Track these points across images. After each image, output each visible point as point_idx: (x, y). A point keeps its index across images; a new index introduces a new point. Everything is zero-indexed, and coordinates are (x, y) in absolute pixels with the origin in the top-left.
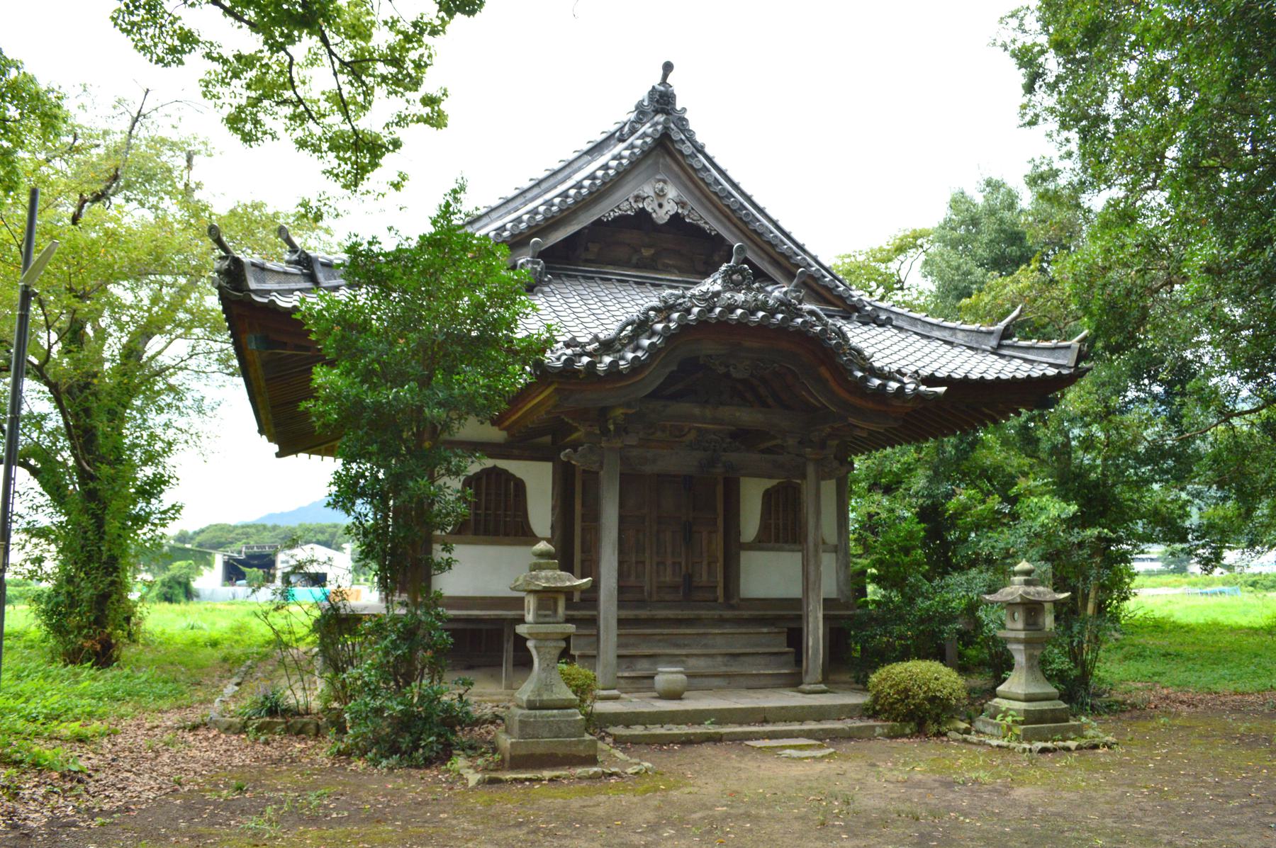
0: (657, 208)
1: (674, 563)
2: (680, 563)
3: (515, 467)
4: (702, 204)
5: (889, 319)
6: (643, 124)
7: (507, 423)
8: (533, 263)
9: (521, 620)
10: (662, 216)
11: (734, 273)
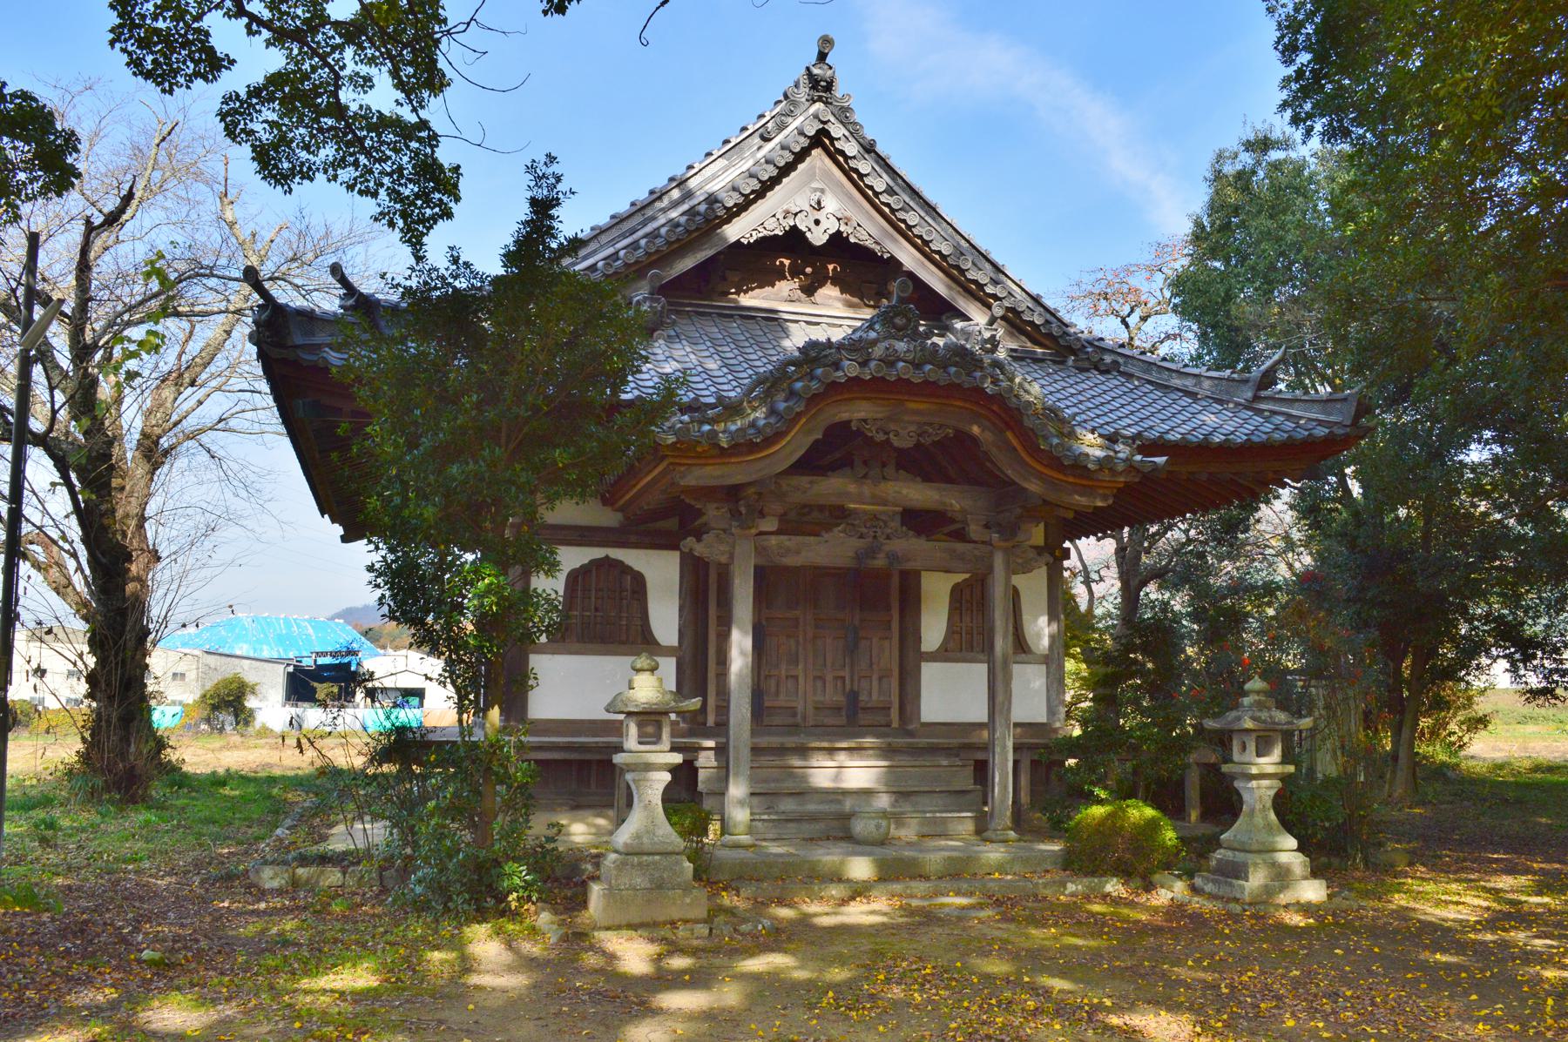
0: (812, 226)
1: (836, 678)
2: (843, 678)
3: (633, 558)
4: (871, 218)
5: (1115, 362)
6: (795, 117)
7: (622, 502)
8: (652, 300)
9: (619, 749)
10: (818, 238)
11: (896, 315)
